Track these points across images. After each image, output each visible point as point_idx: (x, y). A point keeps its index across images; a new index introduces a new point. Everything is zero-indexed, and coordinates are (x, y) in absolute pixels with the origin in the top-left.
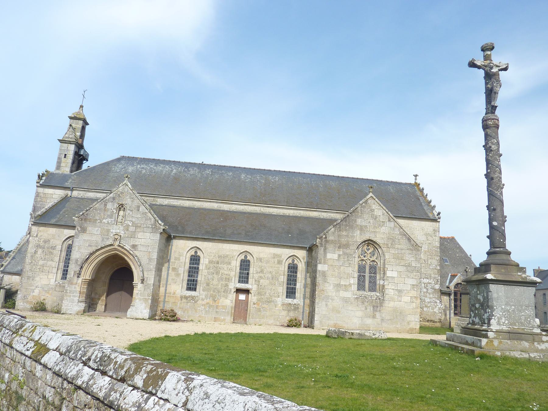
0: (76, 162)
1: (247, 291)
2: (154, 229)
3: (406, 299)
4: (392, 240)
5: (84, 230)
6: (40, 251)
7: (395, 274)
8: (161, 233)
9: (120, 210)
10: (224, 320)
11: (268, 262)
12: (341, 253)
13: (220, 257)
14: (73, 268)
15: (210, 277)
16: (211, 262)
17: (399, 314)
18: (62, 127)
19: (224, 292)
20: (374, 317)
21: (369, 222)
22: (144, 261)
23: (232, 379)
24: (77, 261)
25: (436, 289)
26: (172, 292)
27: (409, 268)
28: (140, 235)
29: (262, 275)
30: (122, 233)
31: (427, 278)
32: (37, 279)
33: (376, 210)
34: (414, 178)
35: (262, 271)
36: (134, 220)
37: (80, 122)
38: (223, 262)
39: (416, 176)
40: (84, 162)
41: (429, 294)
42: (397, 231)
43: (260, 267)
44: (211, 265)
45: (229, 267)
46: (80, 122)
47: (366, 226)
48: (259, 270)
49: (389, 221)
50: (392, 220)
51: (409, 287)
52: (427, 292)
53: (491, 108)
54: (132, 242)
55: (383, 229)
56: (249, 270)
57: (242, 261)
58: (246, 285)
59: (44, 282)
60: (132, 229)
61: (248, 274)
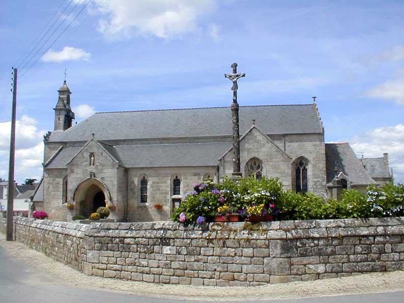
0: (67, 121)
2: (113, 166)
4: (271, 156)
5: (72, 172)
6: (51, 186)
8: (118, 168)
9: (91, 157)
14: (70, 195)
15: (154, 192)
18: (54, 100)
19: (164, 201)
21: (254, 146)
22: (110, 187)
24: (71, 190)
25: (323, 186)
27: (283, 174)
28: (105, 171)
29: (188, 188)
30: (94, 171)
31: (317, 178)
32: (52, 203)
33: (258, 137)
34: (313, 99)
35: (188, 186)
36: (100, 162)
37: (65, 93)
39: (314, 98)
40: (73, 120)
41: (319, 189)
42: (274, 149)
45: (166, 184)
46: (65, 93)
47: (251, 148)
48: (186, 185)
49: (268, 142)
50: (269, 142)
52: (316, 188)
54: (101, 175)
55: (264, 149)
56: (179, 186)
57: (174, 180)
58: (179, 196)
59: (56, 205)
60: (100, 167)
61: (179, 188)
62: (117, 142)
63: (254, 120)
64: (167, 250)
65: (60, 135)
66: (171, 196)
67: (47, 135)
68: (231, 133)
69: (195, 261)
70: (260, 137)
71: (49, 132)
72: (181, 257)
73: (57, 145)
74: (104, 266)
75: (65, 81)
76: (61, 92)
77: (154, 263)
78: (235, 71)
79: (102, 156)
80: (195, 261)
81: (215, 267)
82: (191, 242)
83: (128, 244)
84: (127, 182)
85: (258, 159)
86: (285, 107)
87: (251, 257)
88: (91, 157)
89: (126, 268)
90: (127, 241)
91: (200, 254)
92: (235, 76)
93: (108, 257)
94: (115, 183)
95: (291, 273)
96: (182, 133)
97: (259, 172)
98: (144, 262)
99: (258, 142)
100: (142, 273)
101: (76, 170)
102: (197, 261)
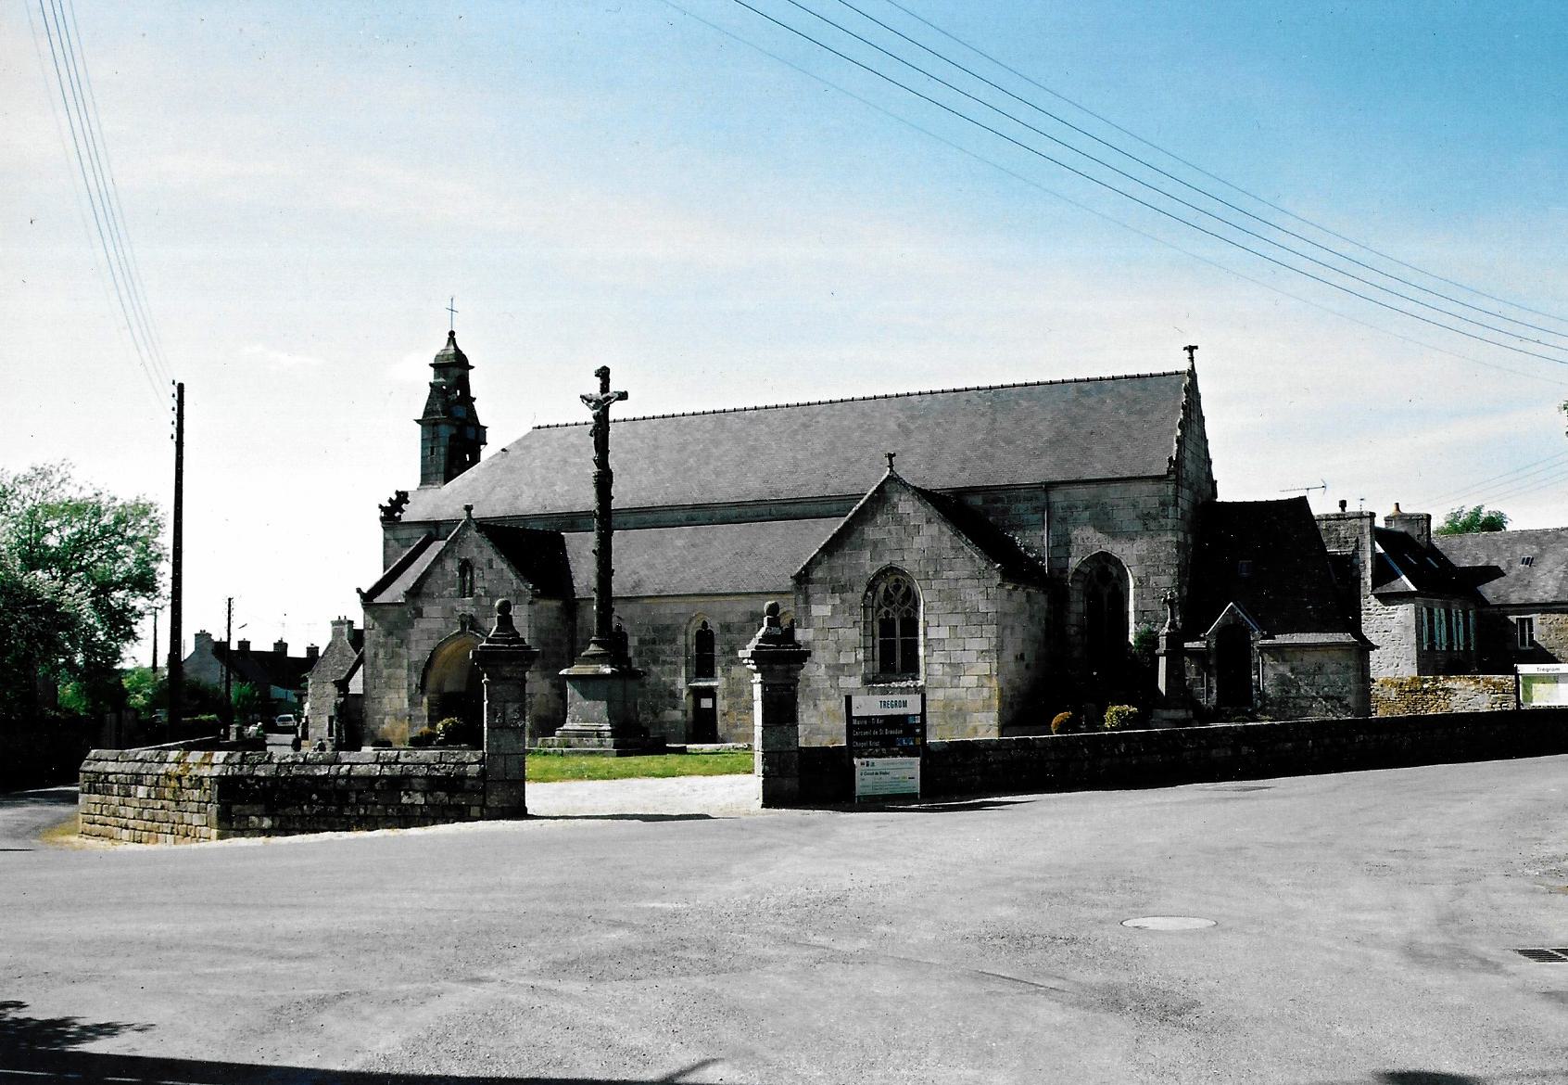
1: (710, 693)
4: (935, 561)
7: (944, 633)
12: (838, 601)
13: (656, 630)
16: (641, 642)
23: (340, 814)
30: (471, 611)
32: (385, 701)
37: (452, 372)
38: (663, 641)
39: (1191, 349)
43: (728, 643)
46: (452, 372)
48: (726, 648)
51: (972, 656)
53: (602, 461)
55: (920, 542)
59: (397, 704)
60: (486, 601)
64: (141, 791)
65: (446, 501)
68: (618, 538)
70: (906, 505)
75: (452, 334)
77: (130, 812)
85: (903, 573)
86: (1087, 386)
88: (463, 574)
95: (230, 823)
96: (752, 487)
97: (908, 612)
99: (899, 520)
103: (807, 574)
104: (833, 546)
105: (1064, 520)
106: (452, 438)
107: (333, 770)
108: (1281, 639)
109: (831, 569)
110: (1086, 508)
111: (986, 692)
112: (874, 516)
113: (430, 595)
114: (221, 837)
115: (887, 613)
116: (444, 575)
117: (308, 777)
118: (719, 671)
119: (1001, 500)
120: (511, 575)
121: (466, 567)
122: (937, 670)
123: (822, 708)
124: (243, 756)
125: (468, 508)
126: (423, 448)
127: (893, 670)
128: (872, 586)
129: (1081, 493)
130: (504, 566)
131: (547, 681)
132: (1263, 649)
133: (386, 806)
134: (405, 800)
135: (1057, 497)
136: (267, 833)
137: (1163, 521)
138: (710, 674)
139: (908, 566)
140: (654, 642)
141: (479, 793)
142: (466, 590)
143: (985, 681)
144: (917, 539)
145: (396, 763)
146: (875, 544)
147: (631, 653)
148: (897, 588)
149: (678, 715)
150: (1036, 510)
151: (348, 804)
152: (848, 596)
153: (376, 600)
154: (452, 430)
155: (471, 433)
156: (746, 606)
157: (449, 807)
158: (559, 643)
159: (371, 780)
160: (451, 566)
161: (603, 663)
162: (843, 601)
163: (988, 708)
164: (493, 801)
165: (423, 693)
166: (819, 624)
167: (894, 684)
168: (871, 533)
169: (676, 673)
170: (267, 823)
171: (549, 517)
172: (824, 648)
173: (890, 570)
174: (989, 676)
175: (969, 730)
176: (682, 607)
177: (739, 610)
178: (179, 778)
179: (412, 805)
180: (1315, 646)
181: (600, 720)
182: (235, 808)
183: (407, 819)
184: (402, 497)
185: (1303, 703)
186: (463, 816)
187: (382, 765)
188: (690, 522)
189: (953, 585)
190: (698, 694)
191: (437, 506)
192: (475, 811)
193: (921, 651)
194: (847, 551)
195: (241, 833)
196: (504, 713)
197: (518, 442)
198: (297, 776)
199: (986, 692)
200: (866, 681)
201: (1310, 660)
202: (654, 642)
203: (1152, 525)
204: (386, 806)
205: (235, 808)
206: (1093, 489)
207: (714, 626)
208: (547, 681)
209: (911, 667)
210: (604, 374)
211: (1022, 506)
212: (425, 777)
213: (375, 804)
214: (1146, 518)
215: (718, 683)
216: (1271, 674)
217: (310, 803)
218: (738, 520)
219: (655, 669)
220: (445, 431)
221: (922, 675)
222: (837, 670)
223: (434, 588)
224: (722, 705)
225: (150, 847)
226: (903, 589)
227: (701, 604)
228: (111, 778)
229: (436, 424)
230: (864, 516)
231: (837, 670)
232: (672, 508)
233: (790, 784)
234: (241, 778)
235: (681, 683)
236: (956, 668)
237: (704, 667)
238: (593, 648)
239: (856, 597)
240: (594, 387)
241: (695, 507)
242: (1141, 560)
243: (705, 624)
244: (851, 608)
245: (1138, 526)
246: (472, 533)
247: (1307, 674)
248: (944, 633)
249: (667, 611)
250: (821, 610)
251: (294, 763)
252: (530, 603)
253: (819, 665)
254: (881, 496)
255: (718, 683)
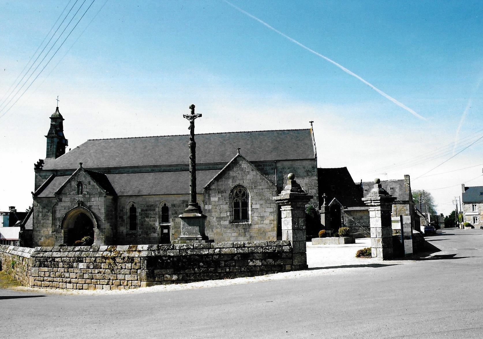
1: (168, 227)
3: (267, 222)
4: (255, 184)
5: (61, 200)
6: (40, 215)
7: (258, 206)
10: (397, 233)
11: (179, 206)
12: (220, 196)
13: (148, 206)
16: (142, 210)
17: (263, 233)
18: (46, 127)
20: (245, 236)
23: (215, 271)
24: (59, 218)
26: (121, 232)
28: (93, 199)
30: (81, 199)
32: (42, 232)
37: (57, 121)
38: (150, 210)
39: (312, 122)
43: (175, 210)
44: (143, 213)
46: (57, 121)
48: (174, 212)
51: (268, 214)
60: (87, 196)
62: (110, 170)
63: (239, 149)
64: (81, 265)
65: (51, 164)
66: (160, 223)
67: (38, 162)
69: (98, 273)
70: (244, 165)
71: (40, 160)
72: (90, 271)
73: (48, 174)
74: (42, 278)
75: (57, 108)
76: (53, 118)
77: (73, 275)
78: (193, 112)
79: (91, 185)
80: (98, 273)
81: (110, 277)
82: (95, 259)
83: (58, 262)
84: (116, 209)
85: (243, 187)
86: (281, 132)
87: (130, 269)
89: (55, 279)
90: (56, 260)
91: (101, 268)
92: (193, 118)
93: (45, 272)
94: (103, 211)
95: (153, 279)
97: (244, 200)
98: (67, 275)
99: (242, 170)
100: (66, 282)
101: (64, 199)
102: (100, 272)
103: (209, 187)
104: (217, 179)
105: (281, 172)
106: (58, 143)
107: (211, 251)
108: (350, 209)
109: (218, 185)
110: (289, 168)
111: (272, 225)
112: (233, 168)
113: (65, 194)
114: (148, 285)
115: (237, 200)
116: (71, 187)
117: (198, 255)
118: (171, 220)
119: (261, 166)
120: (98, 187)
121: (80, 184)
122: (256, 218)
123: (215, 232)
124: (158, 246)
125: (81, 164)
126: (48, 146)
127: (239, 219)
128: (232, 191)
129: (286, 163)
130: (95, 184)
131: (109, 224)
132: (345, 212)
133: (241, 267)
134: (251, 264)
135: (279, 165)
136: (177, 282)
137: (313, 173)
138: (168, 221)
139: (245, 184)
140: (147, 210)
141: (290, 258)
142: (80, 192)
143: (272, 222)
144: (248, 176)
145: (244, 247)
146: (234, 177)
147: (138, 214)
148: (240, 192)
149: (156, 235)
150: (272, 169)
151: (220, 267)
152: (224, 194)
153: (39, 196)
154: (57, 140)
155: (64, 142)
156: (182, 198)
157: (274, 266)
158: (111, 211)
159: (233, 255)
160: (74, 184)
161: (197, 212)
162: (222, 196)
163: (273, 230)
164: (296, 262)
165: (62, 228)
166: (213, 203)
167: (240, 223)
168: (232, 173)
169: (155, 221)
170: (175, 277)
171: (100, 169)
172: (215, 211)
173: (239, 186)
174: (274, 220)
175: (267, 238)
176: (157, 198)
177: (178, 200)
178: (114, 258)
179: (255, 266)
180: (360, 211)
181: (196, 234)
182: (156, 272)
183: (252, 272)
184: (41, 162)
185: (357, 228)
186: (281, 269)
187: (237, 248)
188: (153, 171)
189: (261, 191)
190: (163, 228)
191: (55, 165)
192: (288, 267)
193: (250, 213)
194: (223, 179)
195: (160, 283)
196: (298, 223)
197: (83, 145)
198: (191, 255)
199: (272, 225)
200: (230, 222)
201: (359, 215)
202: (147, 210)
203: (310, 174)
204: (241, 267)
205: (156, 272)
206: (290, 163)
207: (169, 205)
208: (109, 224)
209: (246, 217)
210: (193, 107)
211: (268, 168)
212: (262, 253)
213: (235, 266)
214: (308, 172)
215: (171, 224)
216: (347, 219)
217: (199, 267)
218: (169, 171)
219: (147, 219)
220: (56, 140)
221: (250, 220)
222: (220, 219)
223: (67, 192)
224: (172, 232)
225: (90, 292)
226: (242, 192)
227: (165, 198)
228: (56, 260)
229: (53, 137)
230: (229, 168)
231: (220, 219)
232: (146, 167)
233: (391, 251)
234: (160, 257)
235: (157, 224)
236: (262, 218)
237: (165, 218)
238: (190, 207)
239: (227, 194)
240: (189, 112)
241: (154, 166)
242: (306, 184)
243: (165, 204)
244: (225, 198)
245: (305, 174)
246: (82, 173)
247: (358, 219)
248: (258, 206)
249: (152, 200)
250: (214, 199)
251: (188, 249)
252: (105, 197)
253: (214, 217)
254: (235, 162)
255: (171, 224)
